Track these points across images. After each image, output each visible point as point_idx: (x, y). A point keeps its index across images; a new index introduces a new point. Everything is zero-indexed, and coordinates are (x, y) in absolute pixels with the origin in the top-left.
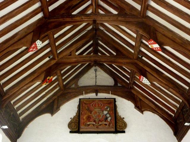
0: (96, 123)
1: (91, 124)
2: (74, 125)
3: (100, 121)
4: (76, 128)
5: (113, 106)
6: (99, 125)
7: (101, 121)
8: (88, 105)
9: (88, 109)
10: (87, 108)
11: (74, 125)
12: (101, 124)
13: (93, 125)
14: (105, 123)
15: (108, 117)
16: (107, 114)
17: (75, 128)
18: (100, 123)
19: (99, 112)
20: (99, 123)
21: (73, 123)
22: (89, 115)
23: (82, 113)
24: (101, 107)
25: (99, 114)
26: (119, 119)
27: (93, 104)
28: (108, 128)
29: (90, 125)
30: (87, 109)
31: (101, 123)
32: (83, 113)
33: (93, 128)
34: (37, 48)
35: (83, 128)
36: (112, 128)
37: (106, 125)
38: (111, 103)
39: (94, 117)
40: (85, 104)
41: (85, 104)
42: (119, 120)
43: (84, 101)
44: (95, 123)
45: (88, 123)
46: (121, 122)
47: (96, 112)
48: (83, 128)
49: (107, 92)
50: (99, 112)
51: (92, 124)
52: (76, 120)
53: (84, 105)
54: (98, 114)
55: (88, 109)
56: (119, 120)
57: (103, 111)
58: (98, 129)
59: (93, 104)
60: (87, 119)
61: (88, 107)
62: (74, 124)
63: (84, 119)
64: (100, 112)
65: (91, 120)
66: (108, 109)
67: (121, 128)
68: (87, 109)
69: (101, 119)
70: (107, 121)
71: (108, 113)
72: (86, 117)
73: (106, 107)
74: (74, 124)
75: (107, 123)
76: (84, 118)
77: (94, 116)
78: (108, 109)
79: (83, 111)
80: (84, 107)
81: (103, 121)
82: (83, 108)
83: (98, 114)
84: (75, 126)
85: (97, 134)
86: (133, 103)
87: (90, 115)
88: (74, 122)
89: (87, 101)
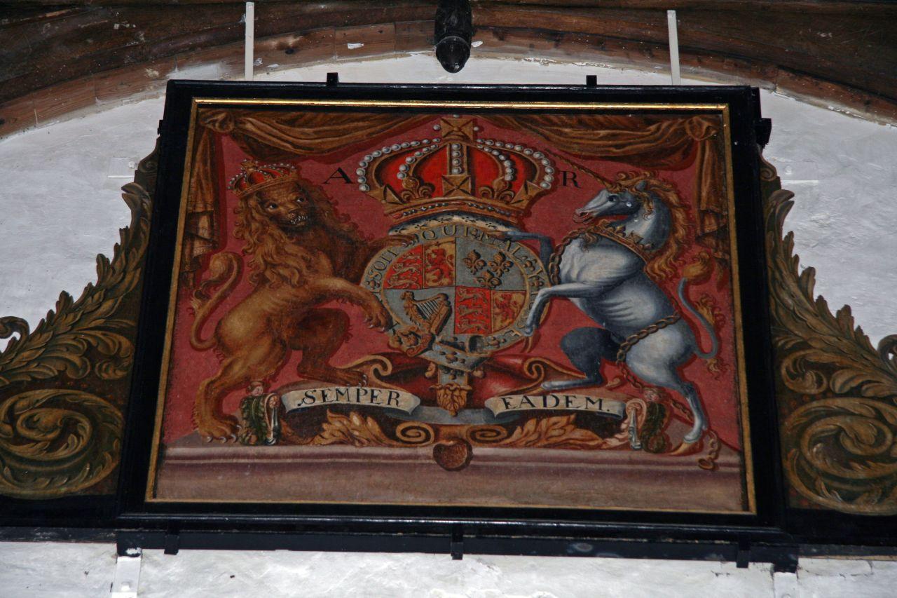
0: (429, 400)
1: (342, 411)
2: (48, 417)
3: (495, 367)
4: (92, 454)
5: (717, 190)
6: (477, 419)
7: (519, 380)
8: (312, 170)
9: (313, 215)
10: (286, 203)
11: (48, 417)
12: (515, 420)
13: (388, 421)
14: (579, 402)
15: (644, 331)
16: (612, 287)
17: (62, 453)
18: (496, 406)
19: (490, 253)
20: (475, 401)
21: (43, 394)
22: (324, 296)
23: (200, 264)
24: (522, 197)
25: (493, 283)
26: (826, 358)
27: (398, 157)
28: (631, 476)
29: (335, 425)
30: (285, 227)
31: (516, 402)
32: (217, 265)
33: (386, 465)
34: (499, 347)
35: (192, 466)
36: (711, 471)
37: (605, 425)
38: (688, 151)
39: (404, 323)
40: (261, 151)
41: (261, 151)
42: (828, 370)
43: (251, 125)
44: (407, 401)
45: (294, 400)
46: (855, 392)
47: (441, 264)
48: (192, 466)
49: (625, 27)
50: (490, 253)
51: (364, 412)
52: (90, 353)
53: (239, 165)
54: (464, 276)
55: (313, 215)
56: (828, 370)
57: (552, 251)
58: (457, 480)
59: (398, 157)
60: (282, 348)
61: (301, 188)
62: (51, 403)
63: (222, 346)
64: (505, 263)
65: (341, 362)
66: (643, 226)
67: (860, 473)
68: (285, 227)
69: (521, 347)
70: (610, 370)
71: (634, 276)
72: (268, 322)
73: (599, 202)
74: (51, 403)
75: (611, 406)
76: (239, 325)
77: (394, 300)
78: (643, 226)
79: (216, 244)
80: (233, 200)
81: (549, 373)
82: (219, 202)
83: (464, 276)
84: (68, 427)
85: (443, 561)
86: (156, 148)
87: (337, 295)
88: (60, 380)
89: (295, 117)
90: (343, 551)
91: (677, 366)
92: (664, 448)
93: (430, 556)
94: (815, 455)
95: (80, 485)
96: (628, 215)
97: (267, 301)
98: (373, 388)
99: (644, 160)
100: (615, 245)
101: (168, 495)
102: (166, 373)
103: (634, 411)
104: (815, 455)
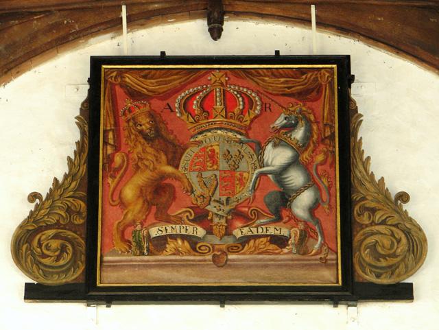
7: (247, 219)
12: (245, 240)
13: (193, 241)
14: (272, 231)
29: (171, 246)
57: (259, 149)
72: (141, 191)
76: (129, 192)
78: (299, 134)
79: (117, 148)
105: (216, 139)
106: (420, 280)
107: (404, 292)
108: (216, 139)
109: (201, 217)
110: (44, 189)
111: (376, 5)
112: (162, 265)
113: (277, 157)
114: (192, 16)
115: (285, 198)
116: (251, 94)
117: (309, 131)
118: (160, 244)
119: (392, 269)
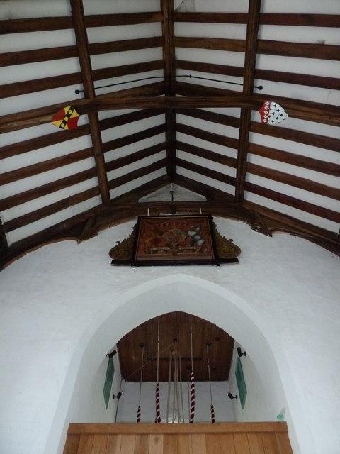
7: (183, 246)
12: (182, 250)
13: (166, 251)
14: (191, 248)
16: (194, 236)
29: (159, 252)
40: (149, 223)
41: (149, 223)
57: (187, 232)
64: (181, 234)
72: (150, 241)
76: (147, 241)
77: (167, 238)
78: (198, 229)
79: (144, 233)
90: (98, 54)
91: (203, 244)
92: (202, 252)
93: (47, 15)
94: (222, 253)
95: (127, 259)
96: (196, 228)
97: (151, 239)
98: (88, 101)
99: (199, 222)
100: (195, 231)
101: (139, 259)
102: (115, 367)
103: (198, 249)
104: (222, 253)
105: (174, 230)
106: (240, 258)
107: (236, 261)
108: (174, 230)
109: (169, 245)
110: (121, 240)
111: (276, 221)
112: (157, 256)
113: (191, 233)
114: (260, 70)
115: (194, 242)
116: (172, 193)
117: (201, 229)
118: (156, 251)
119: (230, 255)
